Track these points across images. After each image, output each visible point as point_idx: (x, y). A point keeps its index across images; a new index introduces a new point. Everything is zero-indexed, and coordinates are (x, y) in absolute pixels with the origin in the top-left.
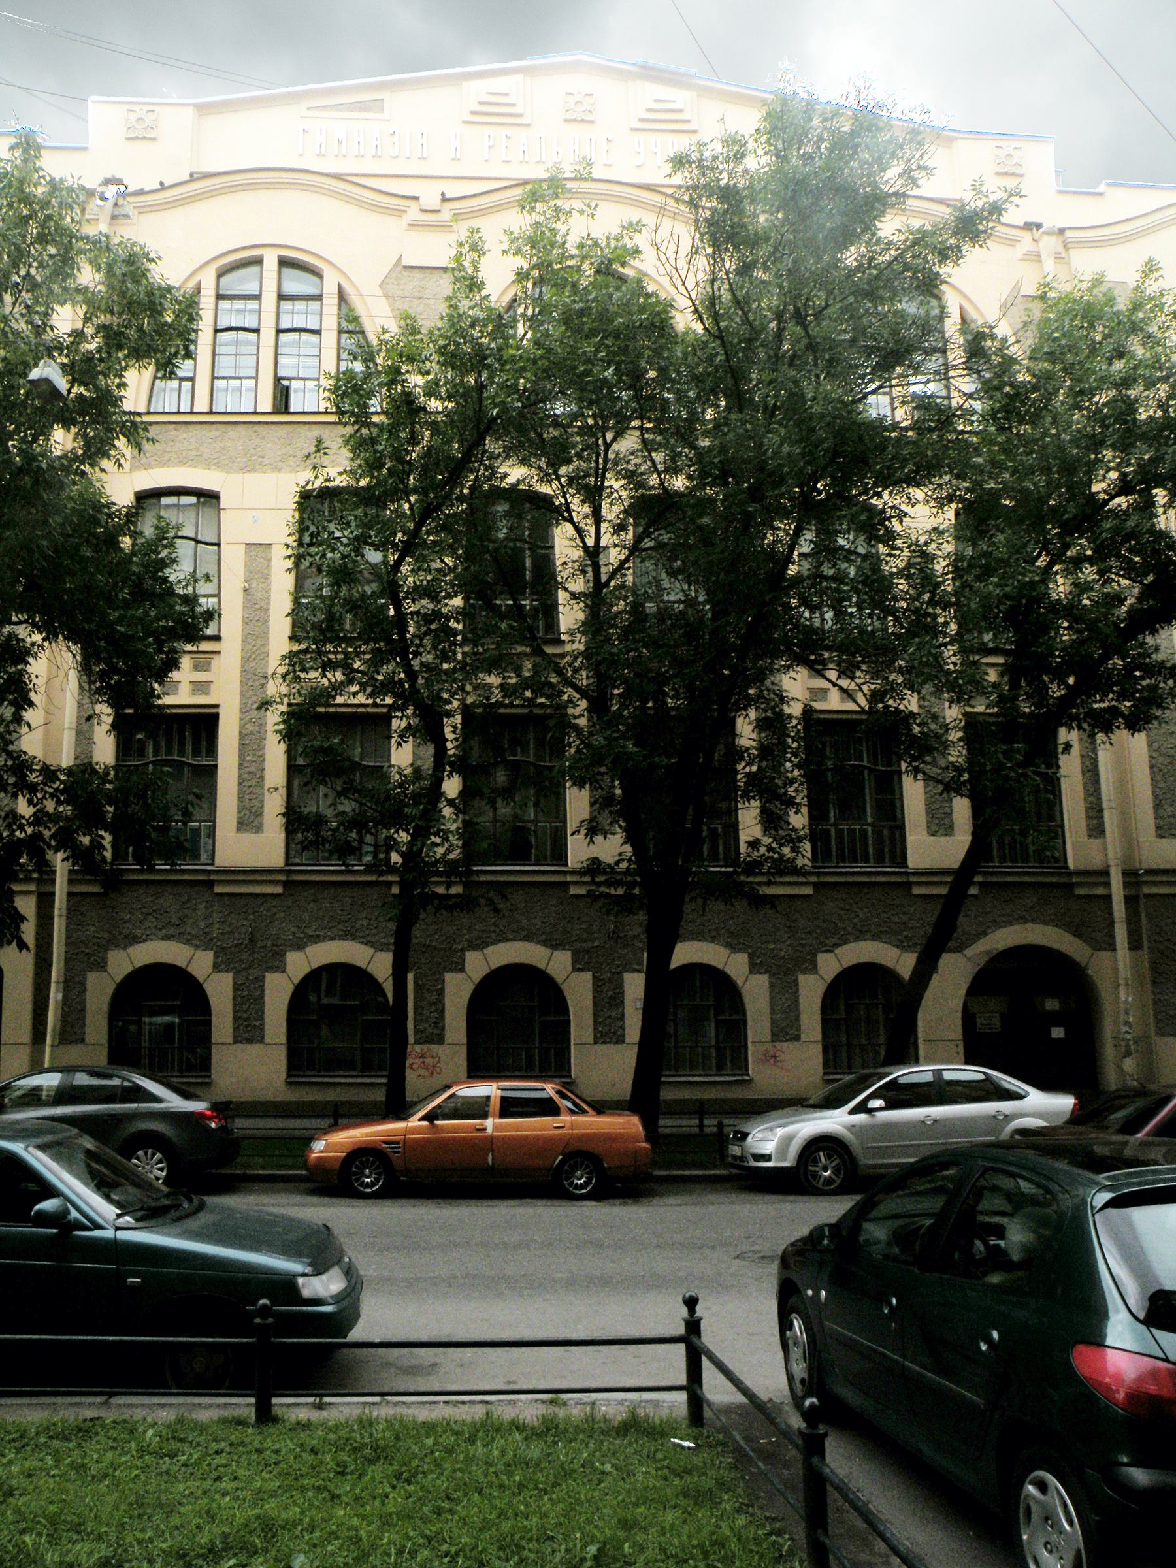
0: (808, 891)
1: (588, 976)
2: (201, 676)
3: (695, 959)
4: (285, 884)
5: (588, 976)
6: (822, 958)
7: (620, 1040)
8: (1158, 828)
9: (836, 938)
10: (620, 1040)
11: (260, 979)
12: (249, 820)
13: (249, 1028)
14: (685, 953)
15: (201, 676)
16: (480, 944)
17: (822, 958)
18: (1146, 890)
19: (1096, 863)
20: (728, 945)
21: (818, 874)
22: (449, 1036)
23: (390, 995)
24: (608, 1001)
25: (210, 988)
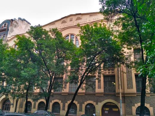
0: (103, 95)
1: (62, 103)
2: (113, 71)
3: (90, 103)
4: (85, 94)
5: (62, 103)
6: (136, 105)
7: (64, 110)
8: (128, 88)
9: (87, 100)
10: (64, 110)
11: (36, 103)
12: (99, 87)
13: (34, 108)
14: (28, 100)
15: (113, 71)
16: (53, 100)
17: (136, 105)
18: (125, 96)
19: (119, 92)
20: (94, 101)
21: (137, 93)
22: (50, 109)
23: (46, 104)
24: (64, 106)
25: (32, 103)
